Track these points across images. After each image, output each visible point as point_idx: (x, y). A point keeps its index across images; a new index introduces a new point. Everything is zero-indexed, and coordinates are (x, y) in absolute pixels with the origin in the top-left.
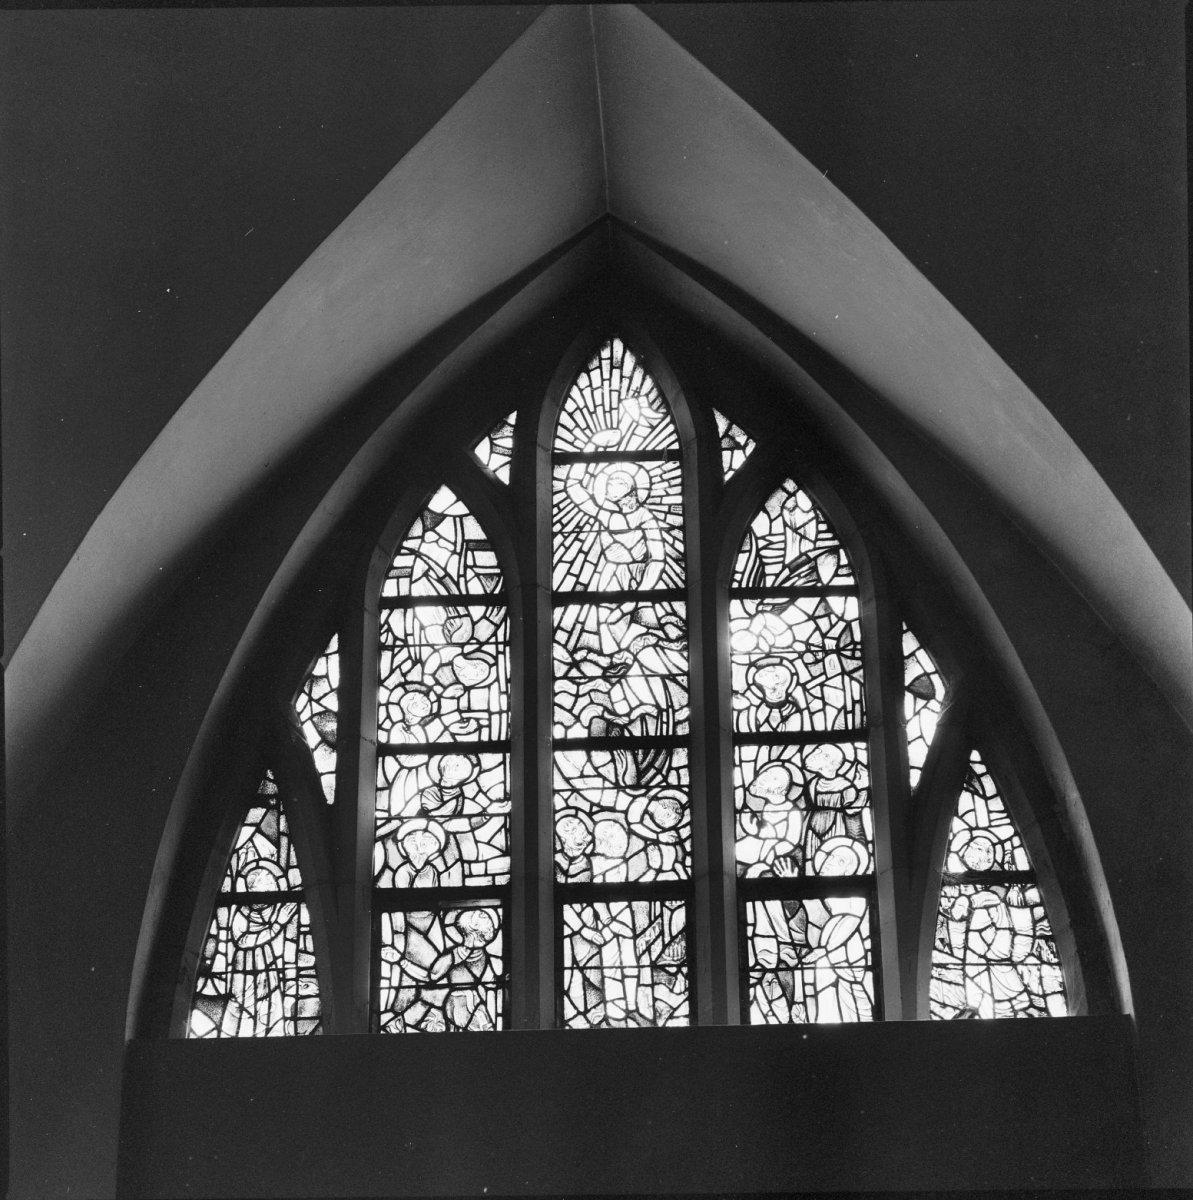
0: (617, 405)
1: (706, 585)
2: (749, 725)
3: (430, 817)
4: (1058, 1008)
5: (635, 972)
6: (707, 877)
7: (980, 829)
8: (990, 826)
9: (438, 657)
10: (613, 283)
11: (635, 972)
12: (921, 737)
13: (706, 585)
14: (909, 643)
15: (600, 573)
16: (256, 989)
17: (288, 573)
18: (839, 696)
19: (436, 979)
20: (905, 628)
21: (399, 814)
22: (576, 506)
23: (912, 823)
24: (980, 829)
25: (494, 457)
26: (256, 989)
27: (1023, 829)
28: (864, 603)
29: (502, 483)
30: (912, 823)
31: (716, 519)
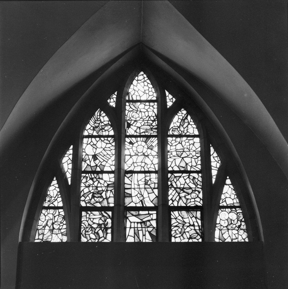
0: (141, 88)
1: (162, 133)
2: (111, 130)
3: (96, 190)
4: (247, 240)
5: (141, 229)
6: (161, 205)
7: (229, 194)
8: (196, 165)
9: (96, 149)
10: (141, 58)
11: (141, 229)
12: (137, 96)
13: (162, 133)
14: (167, 93)
15: (153, 142)
16: (51, 228)
17: (58, 126)
18: (196, 163)
19: (95, 227)
20: (211, 145)
21: (86, 188)
22: (176, 152)
23: (212, 193)
24: (229, 194)
25: (112, 102)
26: (51, 228)
27: (238, 194)
28: (201, 139)
29: (114, 107)
30: (212, 193)
31: (164, 116)
